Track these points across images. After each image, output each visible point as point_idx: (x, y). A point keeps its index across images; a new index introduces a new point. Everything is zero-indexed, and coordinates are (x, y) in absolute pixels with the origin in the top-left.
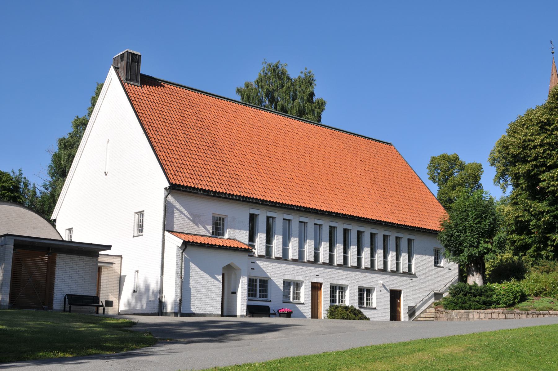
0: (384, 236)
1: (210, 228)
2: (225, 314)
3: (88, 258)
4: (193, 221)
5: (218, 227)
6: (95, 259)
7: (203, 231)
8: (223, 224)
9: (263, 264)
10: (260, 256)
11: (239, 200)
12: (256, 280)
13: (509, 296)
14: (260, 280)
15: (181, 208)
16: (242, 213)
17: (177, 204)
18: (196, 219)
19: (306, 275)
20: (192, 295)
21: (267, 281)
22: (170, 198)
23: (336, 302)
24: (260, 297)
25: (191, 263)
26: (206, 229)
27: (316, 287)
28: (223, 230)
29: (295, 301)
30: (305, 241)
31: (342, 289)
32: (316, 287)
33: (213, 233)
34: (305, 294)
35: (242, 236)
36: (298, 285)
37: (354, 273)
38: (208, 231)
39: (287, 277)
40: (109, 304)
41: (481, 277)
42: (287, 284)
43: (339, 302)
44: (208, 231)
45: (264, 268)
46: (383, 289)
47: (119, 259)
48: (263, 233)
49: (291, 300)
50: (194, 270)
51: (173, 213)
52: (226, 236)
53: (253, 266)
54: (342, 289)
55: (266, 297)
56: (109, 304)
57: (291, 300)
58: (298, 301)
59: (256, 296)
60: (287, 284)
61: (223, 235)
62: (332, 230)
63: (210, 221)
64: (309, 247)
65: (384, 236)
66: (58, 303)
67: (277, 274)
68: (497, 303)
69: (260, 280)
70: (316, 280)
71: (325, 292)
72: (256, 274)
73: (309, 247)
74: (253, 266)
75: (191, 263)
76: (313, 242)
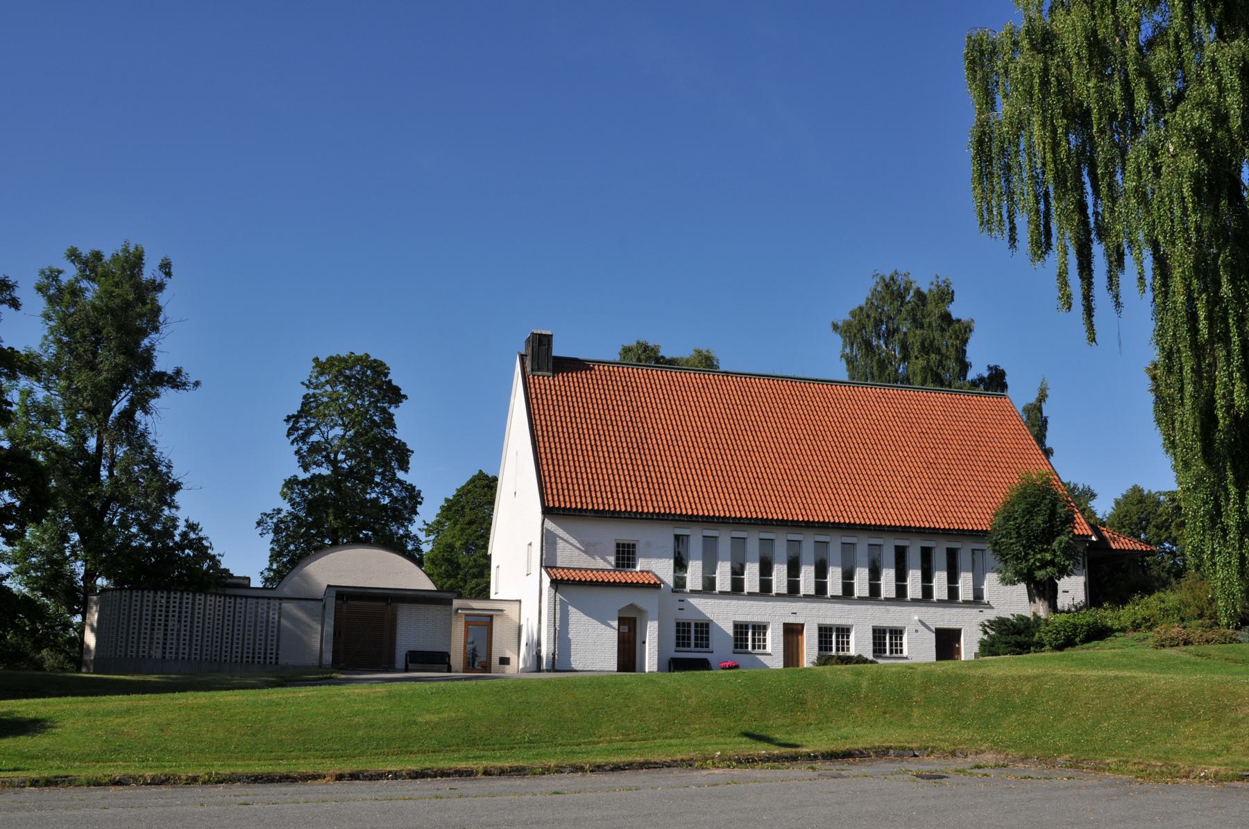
0: (897, 548)
1: (612, 559)
2: (557, 667)
3: (439, 607)
4: (585, 552)
5: (626, 556)
6: (448, 608)
7: (600, 564)
8: (634, 553)
9: (695, 601)
10: (692, 591)
11: (652, 519)
12: (689, 625)
13: (1059, 633)
14: (696, 625)
15: (566, 536)
16: (664, 536)
17: (560, 532)
18: (589, 550)
19: (774, 615)
20: (573, 647)
21: (707, 625)
22: (550, 525)
23: (831, 649)
24: (696, 645)
25: (570, 607)
26: (606, 560)
27: (792, 632)
28: (634, 559)
29: (757, 651)
30: (984, 575)
31: (844, 631)
32: (792, 632)
33: (618, 565)
34: (774, 641)
35: (663, 569)
36: (760, 629)
37: (864, 607)
38: (610, 563)
39: (741, 618)
40: (505, 661)
41: (1046, 603)
42: (740, 629)
43: (838, 650)
44: (610, 563)
45: (700, 608)
46: (921, 628)
47: (517, 605)
48: (889, 568)
49: (750, 648)
50: (575, 615)
51: (555, 543)
52: (638, 569)
53: (681, 605)
54: (844, 631)
55: (707, 646)
56: (505, 661)
57: (750, 648)
58: (761, 651)
59: (689, 645)
60: (740, 629)
61: (634, 566)
62: (926, 554)
63: (613, 549)
64: (888, 579)
65: (897, 548)
66: (400, 660)
67: (723, 614)
68: (1040, 645)
69: (696, 625)
70: (792, 620)
71: (809, 636)
72: (685, 617)
73: (888, 579)
74: (681, 605)
75: (570, 607)
76: (970, 575)
